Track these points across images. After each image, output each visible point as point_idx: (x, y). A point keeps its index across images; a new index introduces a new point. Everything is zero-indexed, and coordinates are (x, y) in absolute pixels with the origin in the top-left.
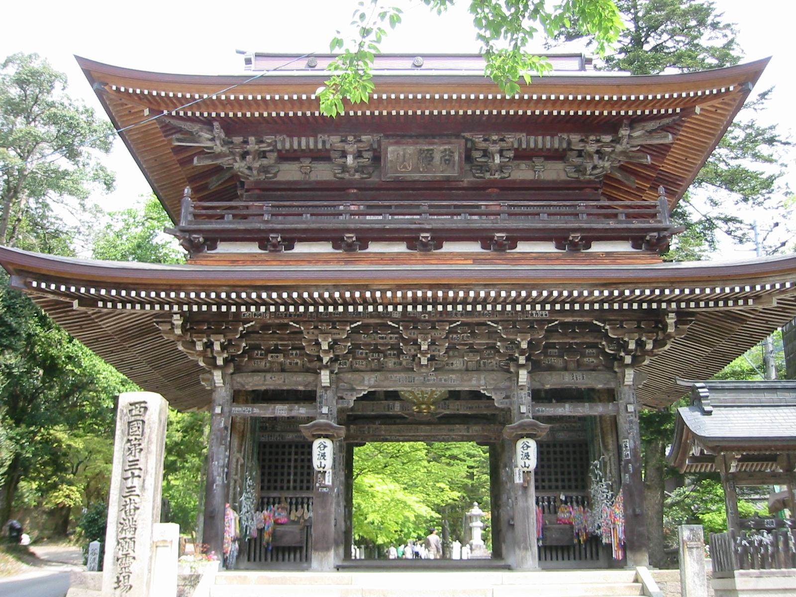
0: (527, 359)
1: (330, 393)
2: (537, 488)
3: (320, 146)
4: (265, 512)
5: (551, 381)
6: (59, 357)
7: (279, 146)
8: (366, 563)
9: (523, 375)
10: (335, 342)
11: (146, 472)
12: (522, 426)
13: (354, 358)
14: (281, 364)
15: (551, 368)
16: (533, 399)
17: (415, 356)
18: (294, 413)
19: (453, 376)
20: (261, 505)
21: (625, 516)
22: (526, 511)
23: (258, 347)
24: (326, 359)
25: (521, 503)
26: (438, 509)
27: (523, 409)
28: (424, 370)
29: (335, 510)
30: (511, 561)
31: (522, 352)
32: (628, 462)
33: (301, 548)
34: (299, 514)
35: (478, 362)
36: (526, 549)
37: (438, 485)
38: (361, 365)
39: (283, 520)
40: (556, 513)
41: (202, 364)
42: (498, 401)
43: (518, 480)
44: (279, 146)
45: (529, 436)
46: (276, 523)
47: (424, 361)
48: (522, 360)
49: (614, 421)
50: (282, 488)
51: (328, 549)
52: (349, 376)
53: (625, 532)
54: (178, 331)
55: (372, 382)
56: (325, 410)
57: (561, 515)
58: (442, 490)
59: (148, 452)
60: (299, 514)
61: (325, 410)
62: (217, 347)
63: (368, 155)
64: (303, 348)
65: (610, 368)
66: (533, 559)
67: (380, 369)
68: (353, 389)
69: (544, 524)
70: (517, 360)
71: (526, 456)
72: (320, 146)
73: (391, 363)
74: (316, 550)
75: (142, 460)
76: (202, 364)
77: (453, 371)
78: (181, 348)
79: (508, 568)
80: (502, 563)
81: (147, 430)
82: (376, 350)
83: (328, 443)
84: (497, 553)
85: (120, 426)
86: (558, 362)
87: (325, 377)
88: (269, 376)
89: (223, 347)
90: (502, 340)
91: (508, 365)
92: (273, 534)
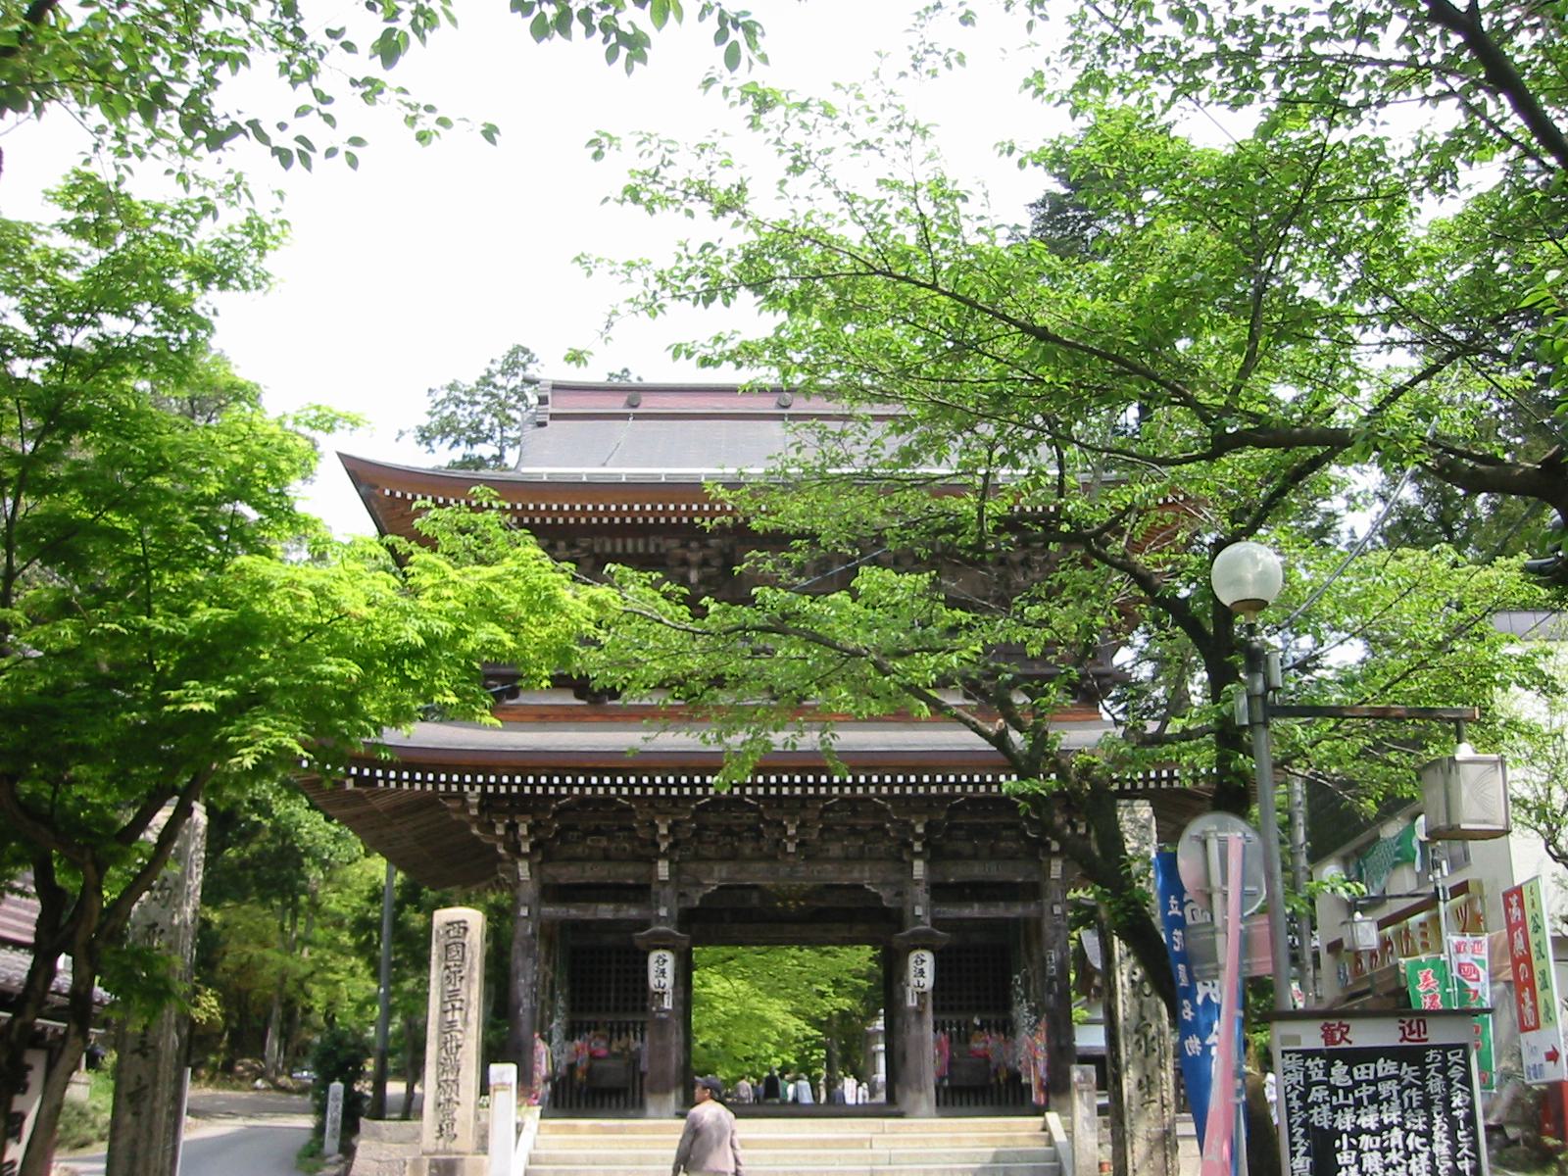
0: (924, 845)
1: (668, 890)
2: (935, 1008)
3: (652, 550)
4: (577, 1042)
5: (956, 873)
6: (239, 802)
7: (597, 549)
8: (759, 1109)
9: (919, 868)
10: (676, 823)
11: (469, 1004)
12: (915, 935)
13: (700, 842)
14: (605, 850)
15: (957, 856)
16: (933, 897)
17: (779, 841)
18: (622, 915)
19: (829, 867)
20: (571, 1033)
21: (1049, 1049)
22: (921, 1041)
23: (573, 828)
24: (664, 846)
25: (914, 1032)
26: (815, 1022)
27: (919, 911)
28: (790, 859)
29: (675, 1038)
30: (903, 1107)
31: (918, 837)
32: (1052, 979)
33: (626, 1090)
34: (623, 1044)
35: (862, 848)
36: (920, 1091)
37: (816, 987)
38: (709, 851)
39: (603, 1052)
40: (968, 1041)
41: (501, 851)
42: (887, 898)
43: (911, 1002)
44: (597, 549)
45: (924, 947)
46: (593, 1056)
47: (791, 848)
48: (918, 847)
49: (1038, 922)
50: (599, 1009)
51: (666, 1091)
52: (693, 866)
53: (1048, 1069)
54: (474, 812)
55: (724, 875)
56: (663, 912)
57: (977, 1045)
58: (822, 995)
59: (471, 980)
60: (623, 1044)
61: (663, 912)
62: (523, 830)
63: (717, 562)
64: (633, 829)
65: (1032, 856)
66: (929, 1101)
67: (734, 856)
68: (699, 884)
69: (951, 1057)
70: (911, 846)
71: (922, 971)
72: (652, 550)
73: (747, 849)
74: (653, 1091)
75: (464, 990)
76: (501, 851)
77: (829, 860)
78: (475, 831)
79: (901, 1115)
80: (895, 1109)
81: (468, 955)
82: (728, 831)
83: (669, 956)
84: (891, 1097)
85: (435, 950)
86: (966, 848)
87: (663, 869)
88: (588, 866)
89: (531, 830)
90: (892, 821)
91: (900, 851)
92: (589, 1071)
